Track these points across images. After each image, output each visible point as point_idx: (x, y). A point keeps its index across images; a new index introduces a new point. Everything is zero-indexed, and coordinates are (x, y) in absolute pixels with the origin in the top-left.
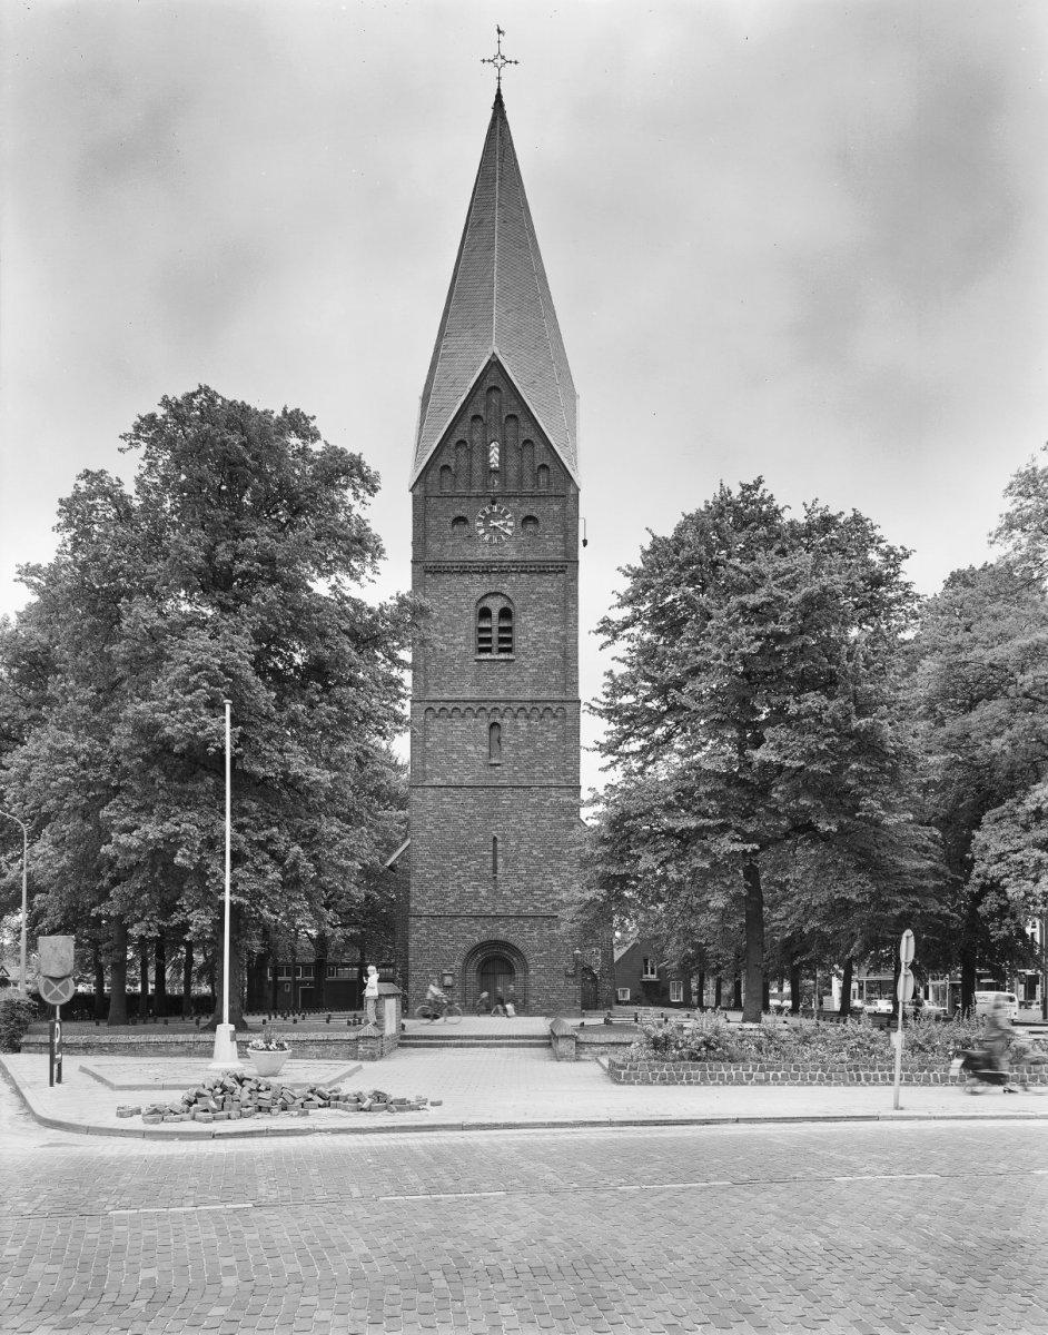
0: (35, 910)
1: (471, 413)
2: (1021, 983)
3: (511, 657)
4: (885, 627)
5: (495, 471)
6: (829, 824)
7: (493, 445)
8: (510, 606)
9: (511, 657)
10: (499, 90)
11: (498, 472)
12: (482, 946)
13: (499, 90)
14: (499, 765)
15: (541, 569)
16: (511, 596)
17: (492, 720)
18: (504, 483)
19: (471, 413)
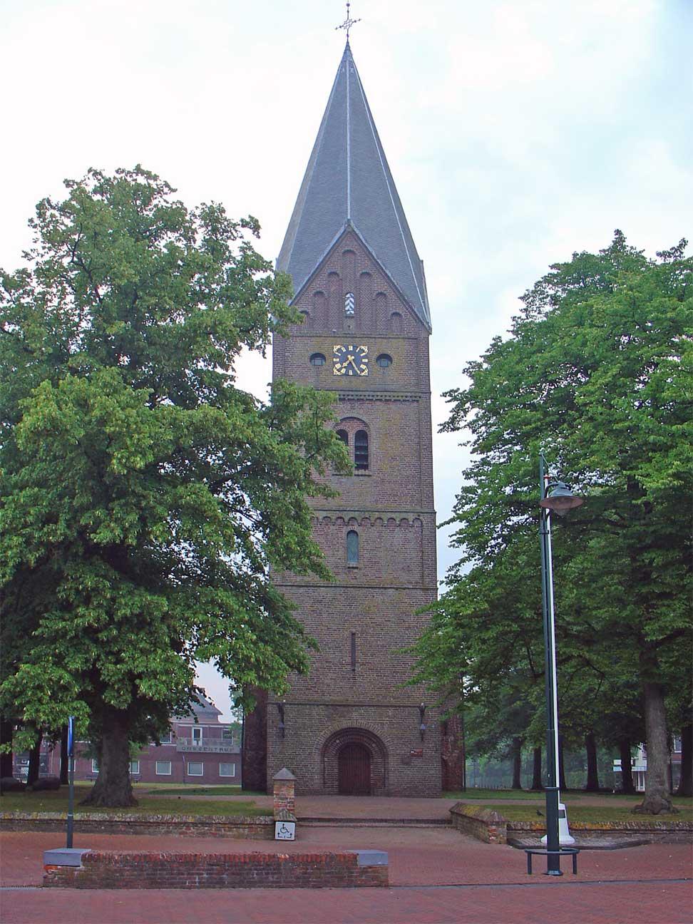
0: (274, 264)
1: (327, 270)
2: (146, 465)
3: (367, 472)
4: (180, 313)
5: (351, 317)
6: (147, 215)
7: (348, 296)
8: (365, 429)
9: (367, 472)
10: (348, 42)
11: (353, 317)
12: (336, 735)
13: (348, 42)
14: (357, 568)
15: (426, 393)
16: (367, 421)
17: (350, 528)
18: (359, 326)
19: (327, 270)
